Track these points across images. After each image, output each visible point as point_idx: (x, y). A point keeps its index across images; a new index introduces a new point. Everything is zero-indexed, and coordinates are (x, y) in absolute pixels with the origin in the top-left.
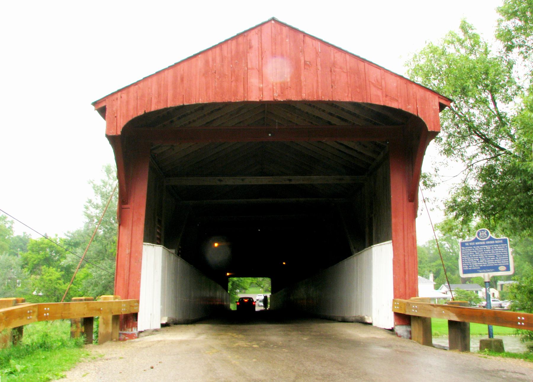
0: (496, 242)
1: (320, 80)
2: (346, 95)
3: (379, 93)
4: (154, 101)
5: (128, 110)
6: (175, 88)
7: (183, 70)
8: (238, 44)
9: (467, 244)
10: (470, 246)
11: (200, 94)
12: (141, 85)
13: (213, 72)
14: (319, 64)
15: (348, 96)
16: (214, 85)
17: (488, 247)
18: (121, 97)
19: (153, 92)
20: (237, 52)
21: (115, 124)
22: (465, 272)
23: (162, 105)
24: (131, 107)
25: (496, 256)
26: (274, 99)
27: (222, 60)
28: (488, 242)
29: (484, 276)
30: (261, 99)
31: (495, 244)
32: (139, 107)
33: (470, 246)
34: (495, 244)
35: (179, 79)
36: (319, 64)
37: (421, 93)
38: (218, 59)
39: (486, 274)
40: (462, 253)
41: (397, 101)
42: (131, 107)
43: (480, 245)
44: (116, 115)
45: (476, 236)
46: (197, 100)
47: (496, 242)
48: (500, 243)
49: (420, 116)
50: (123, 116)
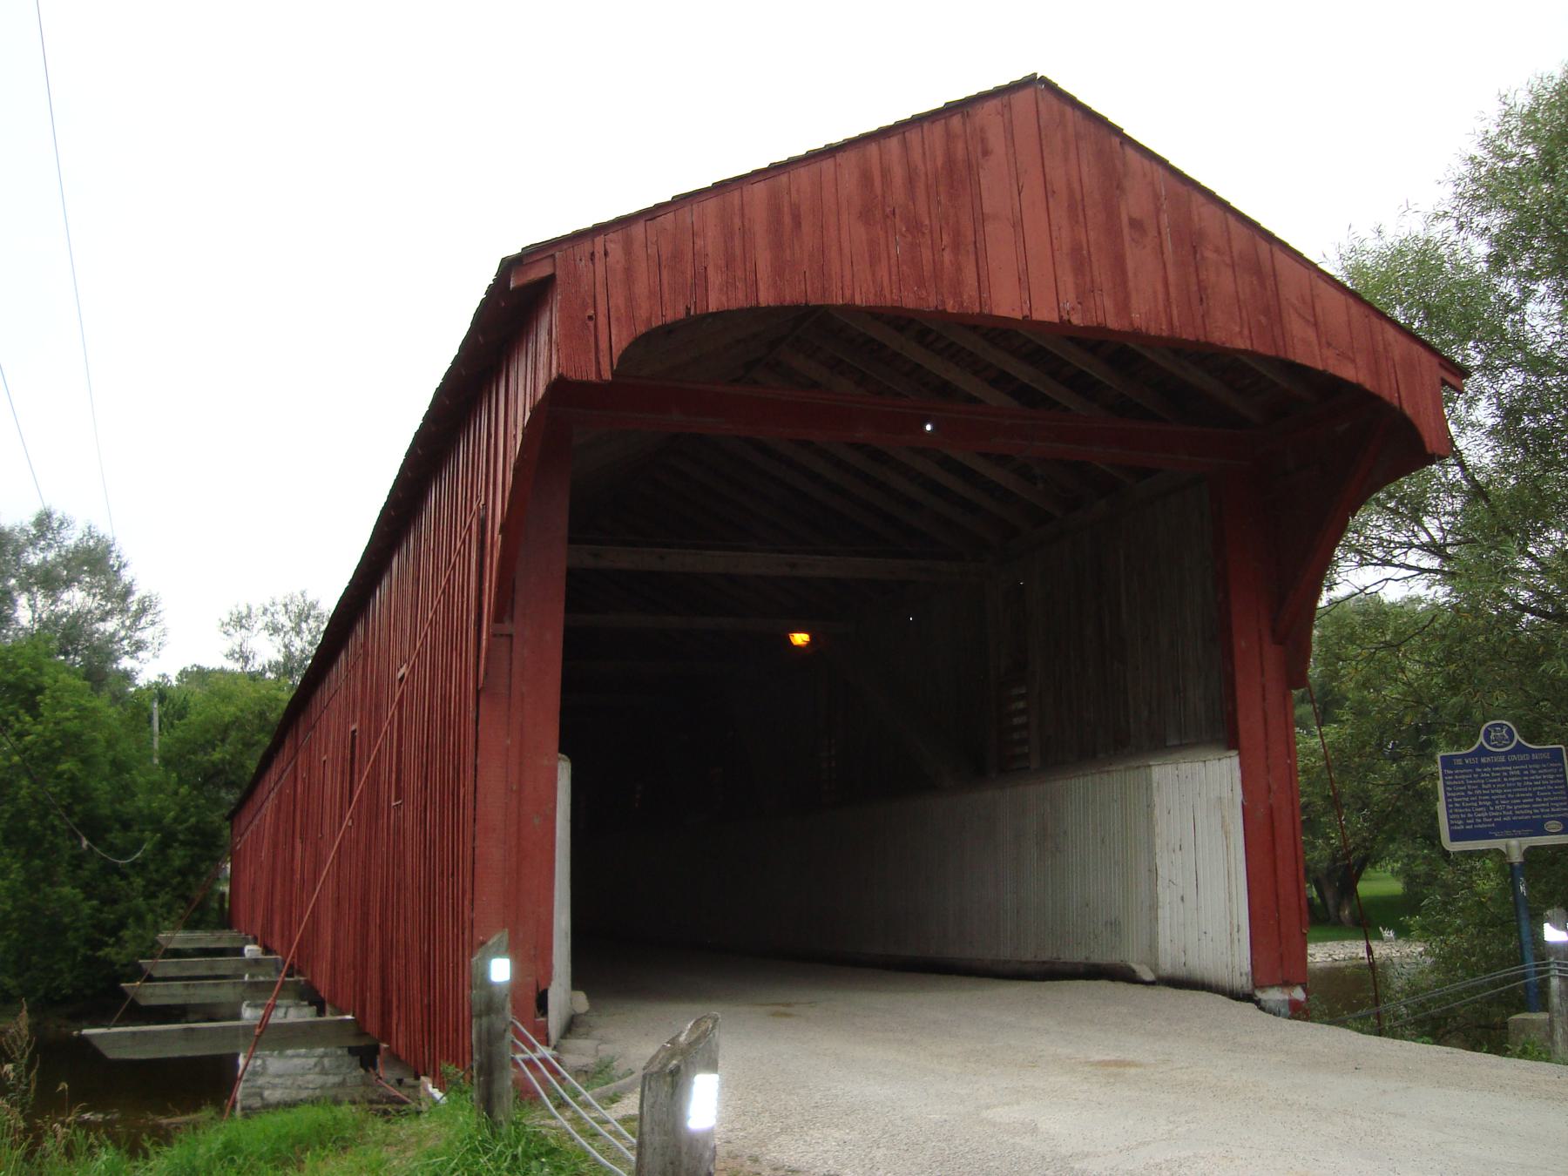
0: (1535, 757)
1: (1172, 278)
2: (1237, 329)
3: (1311, 334)
4: (715, 279)
5: (630, 299)
6: (777, 245)
7: (798, 191)
8: (905, 145)
9: (1459, 762)
10: (1464, 766)
11: (859, 277)
12: (667, 220)
13: (888, 210)
14: (1166, 231)
15: (1241, 332)
16: (893, 252)
17: (1514, 771)
18: (606, 254)
19: (710, 250)
20: (950, 161)
21: (1244, 314)
22: (1456, 836)
23: (741, 296)
24: (641, 288)
25: (1534, 796)
26: (1061, 318)
27: (910, 180)
28: (1514, 758)
29: (1507, 846)
30: (1027, 312)
31: (1532, 762)
32: (666, 296)
33: (1464, 766)
34: (1532, 762)
35: (787, 219)
36: (1166, 231)
37: (1399, 344)
38: (898, 173)
39: (1514, 842)
40: (1445, 786)
41: (1353, 361)
42: (641, 288)
43: (1491, 765)
44: (591, 312)
45: (1481, 739)
46: (848, 294)
47: (1535, 757)
48: (1545, 761)
49: (1408, 411)
50: (618, 319)
